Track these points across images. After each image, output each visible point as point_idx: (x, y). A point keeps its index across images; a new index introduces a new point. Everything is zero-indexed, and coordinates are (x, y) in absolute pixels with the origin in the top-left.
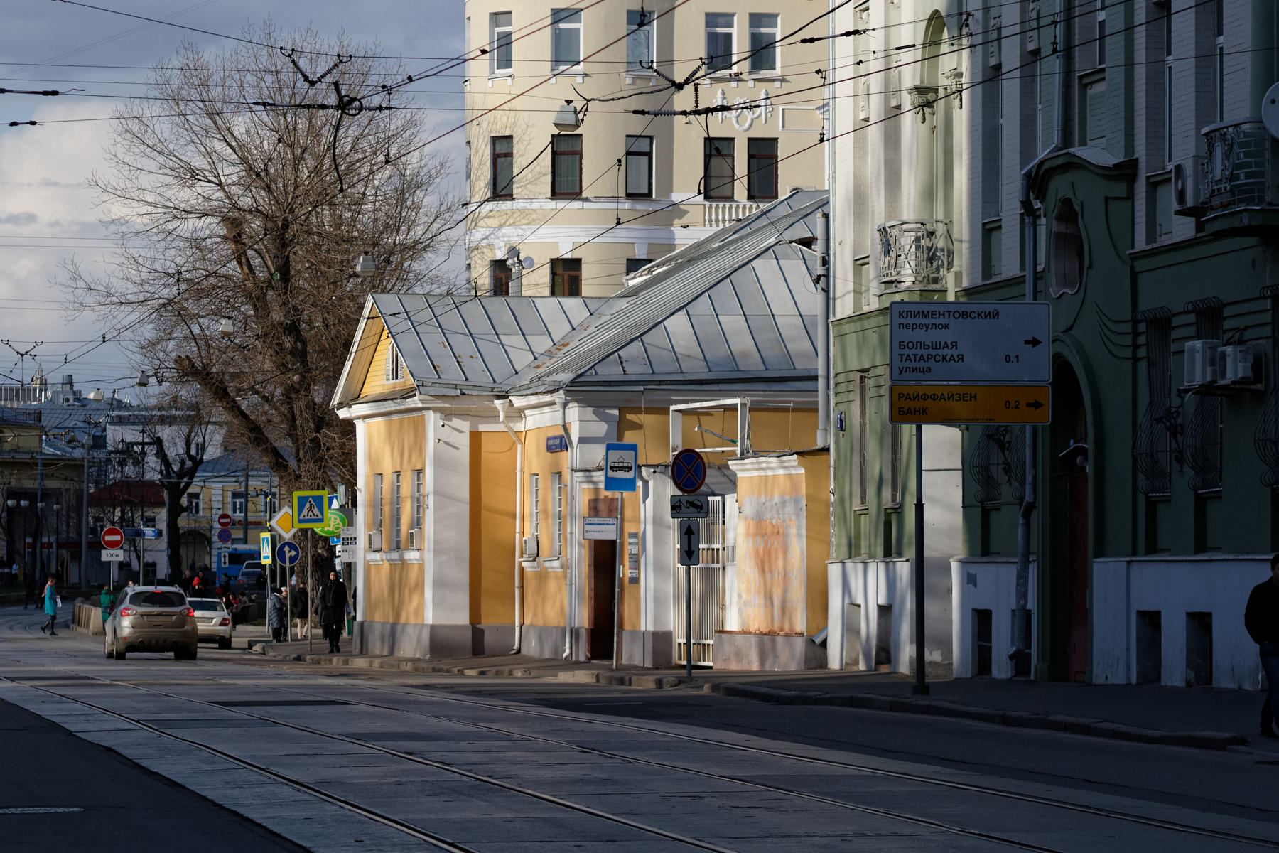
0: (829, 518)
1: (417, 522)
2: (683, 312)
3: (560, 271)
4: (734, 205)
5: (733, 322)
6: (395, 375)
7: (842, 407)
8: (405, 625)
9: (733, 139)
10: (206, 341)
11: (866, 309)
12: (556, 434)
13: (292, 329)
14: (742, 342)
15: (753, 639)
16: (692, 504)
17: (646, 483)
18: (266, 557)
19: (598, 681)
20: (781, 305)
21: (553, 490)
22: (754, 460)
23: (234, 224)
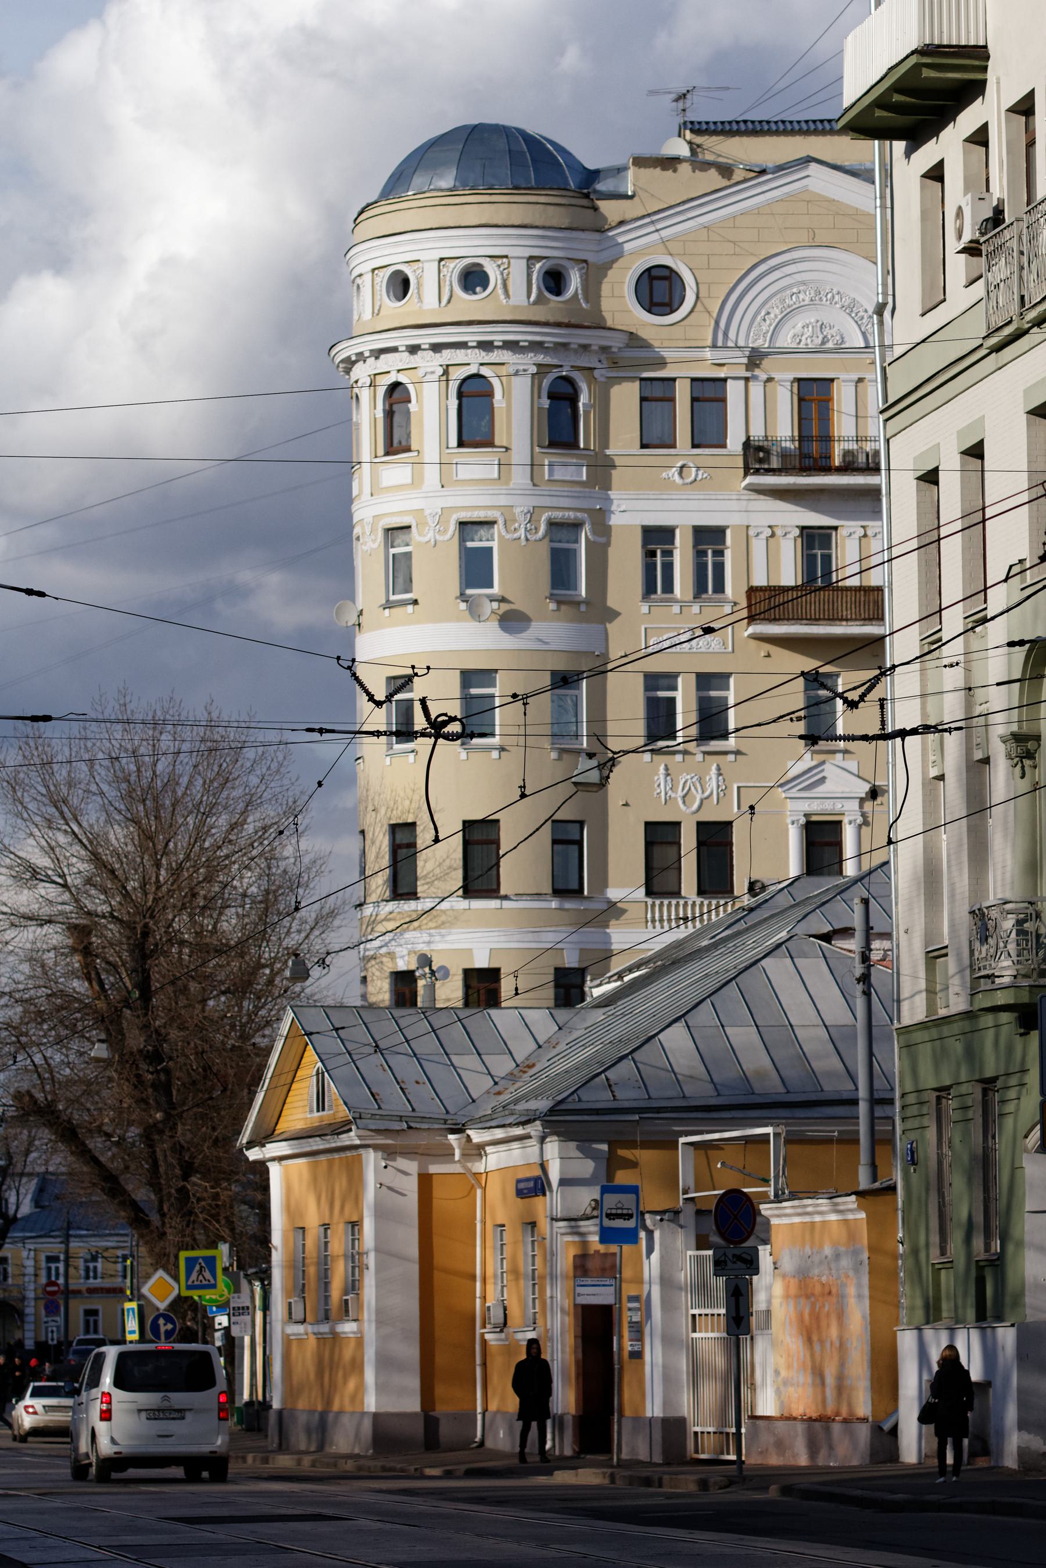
0: (897, 1274)
1: (353, 1286)
2: (681, 1024)
3: (474, 983)
4: (682, 902)
5: (743, 1036)
6: (321, 1106)
7: (913, 1135)
8: (340, 1413)
9: (678, 824)
10: (45, 1073)
11: (942, 1012)
12: (528, 1175)
13: (155, 1057)
14: (755, 1059)
15: (800, 1427)
17: (650, 1233)
18: (133, 1332)
19: (613, 1481)
20: (800, 1012)
21: (524, 1242)
22: (796, 1203)
23: (81, 934)
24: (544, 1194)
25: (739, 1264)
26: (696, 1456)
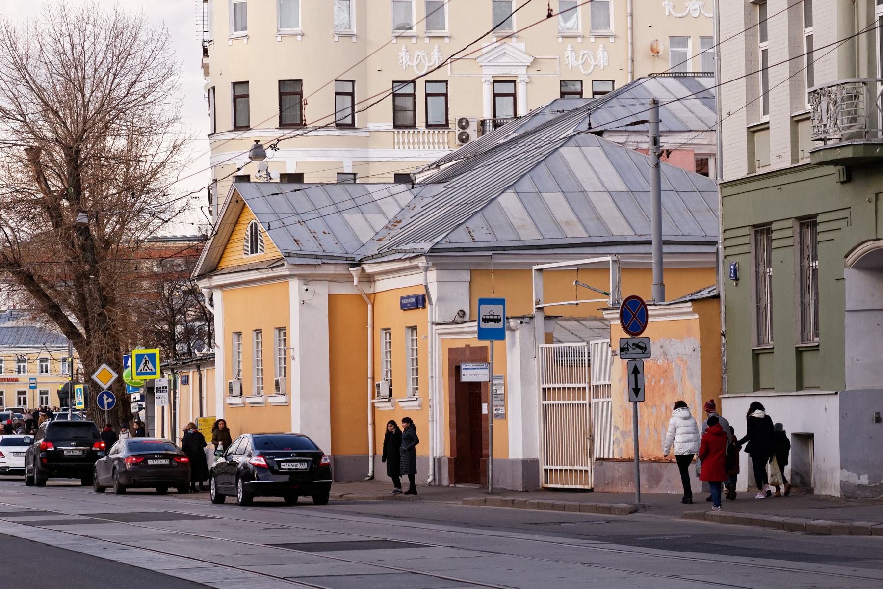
4: (416, 131)
16: (638, 346)
18: (81, 404)
24: (424, 307)
25: (638, 351)
26: (546, 486)
